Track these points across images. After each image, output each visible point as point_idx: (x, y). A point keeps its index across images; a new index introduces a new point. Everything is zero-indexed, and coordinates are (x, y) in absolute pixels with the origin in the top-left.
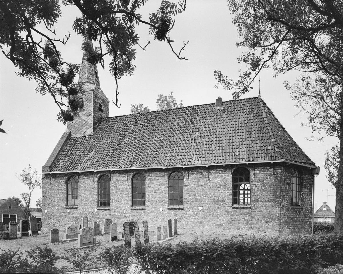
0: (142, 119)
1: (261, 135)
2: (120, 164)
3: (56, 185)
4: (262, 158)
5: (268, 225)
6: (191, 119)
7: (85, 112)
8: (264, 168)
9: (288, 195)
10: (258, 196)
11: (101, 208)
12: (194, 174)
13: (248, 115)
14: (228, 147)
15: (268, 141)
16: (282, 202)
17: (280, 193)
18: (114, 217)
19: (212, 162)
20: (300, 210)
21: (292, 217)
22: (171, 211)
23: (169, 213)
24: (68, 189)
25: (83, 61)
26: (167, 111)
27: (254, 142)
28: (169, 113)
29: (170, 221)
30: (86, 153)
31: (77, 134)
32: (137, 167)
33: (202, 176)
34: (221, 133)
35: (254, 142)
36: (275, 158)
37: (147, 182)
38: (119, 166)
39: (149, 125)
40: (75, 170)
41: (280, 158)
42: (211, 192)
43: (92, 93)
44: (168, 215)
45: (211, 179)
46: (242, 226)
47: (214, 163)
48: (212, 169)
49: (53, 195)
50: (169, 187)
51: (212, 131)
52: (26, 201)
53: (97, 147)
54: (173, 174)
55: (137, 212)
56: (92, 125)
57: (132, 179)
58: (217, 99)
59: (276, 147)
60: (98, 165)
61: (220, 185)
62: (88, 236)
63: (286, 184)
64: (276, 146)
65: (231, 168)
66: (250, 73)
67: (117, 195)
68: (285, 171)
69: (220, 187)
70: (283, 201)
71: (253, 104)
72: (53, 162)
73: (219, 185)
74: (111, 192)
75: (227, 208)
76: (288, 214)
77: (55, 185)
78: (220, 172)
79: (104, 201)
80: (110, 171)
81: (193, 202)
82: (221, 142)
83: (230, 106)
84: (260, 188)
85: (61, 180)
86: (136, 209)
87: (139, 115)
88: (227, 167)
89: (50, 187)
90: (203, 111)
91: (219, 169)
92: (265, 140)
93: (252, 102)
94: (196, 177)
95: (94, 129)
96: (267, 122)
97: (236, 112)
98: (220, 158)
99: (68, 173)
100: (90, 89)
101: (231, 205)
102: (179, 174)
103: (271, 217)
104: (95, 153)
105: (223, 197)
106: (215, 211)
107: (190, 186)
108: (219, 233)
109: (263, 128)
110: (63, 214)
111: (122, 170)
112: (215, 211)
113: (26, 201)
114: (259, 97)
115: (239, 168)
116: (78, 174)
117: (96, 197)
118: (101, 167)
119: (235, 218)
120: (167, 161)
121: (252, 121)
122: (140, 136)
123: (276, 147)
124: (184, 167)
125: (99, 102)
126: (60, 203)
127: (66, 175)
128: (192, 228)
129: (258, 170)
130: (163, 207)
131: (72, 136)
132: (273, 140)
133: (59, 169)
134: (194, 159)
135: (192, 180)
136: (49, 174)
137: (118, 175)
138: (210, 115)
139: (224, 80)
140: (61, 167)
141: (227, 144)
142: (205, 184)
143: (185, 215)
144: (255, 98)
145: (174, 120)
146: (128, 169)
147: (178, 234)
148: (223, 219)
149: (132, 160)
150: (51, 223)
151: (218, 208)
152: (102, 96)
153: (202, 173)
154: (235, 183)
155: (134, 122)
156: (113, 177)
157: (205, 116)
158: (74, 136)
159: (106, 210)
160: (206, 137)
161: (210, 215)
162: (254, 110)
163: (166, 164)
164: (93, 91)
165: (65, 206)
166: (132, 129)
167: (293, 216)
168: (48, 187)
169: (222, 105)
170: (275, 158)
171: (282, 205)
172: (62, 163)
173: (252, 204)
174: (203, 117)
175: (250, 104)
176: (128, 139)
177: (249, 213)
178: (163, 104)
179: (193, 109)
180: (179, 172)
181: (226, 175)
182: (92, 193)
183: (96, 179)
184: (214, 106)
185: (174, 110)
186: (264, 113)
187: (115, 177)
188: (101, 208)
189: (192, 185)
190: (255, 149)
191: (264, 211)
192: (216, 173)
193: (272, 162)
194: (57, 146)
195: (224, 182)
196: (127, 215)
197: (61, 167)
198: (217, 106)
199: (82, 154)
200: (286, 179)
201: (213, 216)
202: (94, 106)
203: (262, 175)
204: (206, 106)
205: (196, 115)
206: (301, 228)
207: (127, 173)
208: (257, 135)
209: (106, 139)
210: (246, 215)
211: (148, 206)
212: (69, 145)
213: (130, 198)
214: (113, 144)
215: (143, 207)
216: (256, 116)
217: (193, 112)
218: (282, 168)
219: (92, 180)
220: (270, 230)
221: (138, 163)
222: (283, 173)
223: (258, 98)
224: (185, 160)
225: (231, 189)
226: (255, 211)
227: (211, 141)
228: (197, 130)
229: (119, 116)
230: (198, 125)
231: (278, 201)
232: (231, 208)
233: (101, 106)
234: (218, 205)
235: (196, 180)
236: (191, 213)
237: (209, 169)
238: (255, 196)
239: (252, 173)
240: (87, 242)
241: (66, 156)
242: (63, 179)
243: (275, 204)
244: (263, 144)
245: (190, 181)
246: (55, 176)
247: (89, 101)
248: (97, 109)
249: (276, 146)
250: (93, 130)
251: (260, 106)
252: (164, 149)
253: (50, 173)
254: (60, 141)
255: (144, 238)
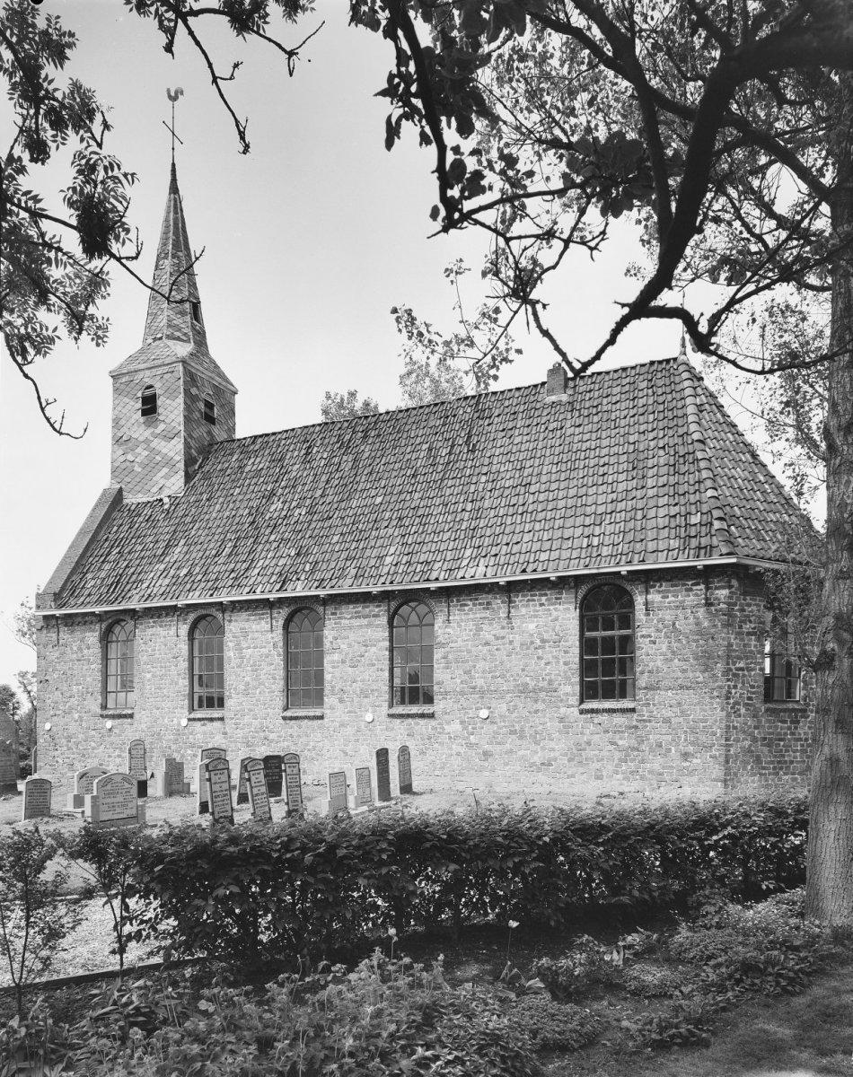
0: (327, 441)
1: (672, 480)
2: (251, 582)
3: (75, 648)
4: (670, 553)
5: (688, 764)
6: (469, 437)
7: (162, 427)
8: (676, 586)
9: (754, 669)
10: (658, 672)
11: (199, 715)
12: (466, 608)
13: (641, 418)
14: (569, 522)
15: (693, 498)
16: (733, 691)
17: (728, 664)
18: (235, 742)
19: (518, 571)
20: (796, 717)
21: (770, 739)
22: (399, 721)
23: (393, 729)
24: (107, 659)
25: (158, 272)
26: (401, 415)
27: (652, 503)
28: (405, 421)
29: (382, 755)
30: (160, 552)
31: (140, 495)
32: (298, 589)
33: (487, 614)
34: (554, 477)
35: (652, 503)
36: (711, 551)
37: (329, 633)
38: (247, 589)
39: (345, 458)
40: (123, 603)
41: (724, 551)
42: (515, 664)
43: (181, 368)
44: (387, 733)
45: (516, 622)
46: (610, 767)
47: (524, 571)
48: (519, 591)
49: (67, 677)
50: (391, 650)
51: (527, 472)
52: (29, 692)
53: (193, 533)
54: (405, 610)
55: (300, 727)
56: (181, 465)
57: (286, 627)
58: (550, 371)
59: (715, 516)
60: (188, 586)
61: (543, 641)
62: (120, 798)
63: (749, 634)
64: (716, 513)
65: (577, 587)
66: (497, 311)
67: (244, 674)
68: (745, 594)
69: (544, 648)
70: (735, 687)
71: (660, 383)
72: (66, 581)
73: (538, 641)
74: (226, 666)
75: (563, 710)
76: (756, 728)
77: (71, 649)
78: (544, 598)
79: (208, 696)
80: (221, 603)
81: (462, 693)
82: (550, 507)
83: (590, 391)
84: (664, 648)
85: (87, 634)
86: (296, 718)
87: (318, 428)
88: (562, 584)
89: (57, 654)
90: (507, 410)
91: (539, 590)
92: (684, 494)
93: (659, 375)
94: (471, 616)
95: (188, 477)
96: (696, 436)
97: (605, 408)
98: (544, 556)
99: (106, 612)
100: (174, 359)
101: (577, 703)
102: (422, 609)
103: (698, 739)
104: (186, 549)
105: (553, 677)
106: (527, 720)
107: (452, 645)
108: (541, 790)
109: (684, 456)
110: (93, 733)
111: (257, 600)
112: (527, 720)
113: (29, 692)
114: (683, 357)
115: (599, 586)
116: (132, 613)
117: (184, 683)
118: (197, 593)
119: (589, 743)
120: (386, 570)
121: (651, 435)
122: (317, 495)
123: (715, 516)
124: (433, 586)
125: (203, 396)
126: (85, 700)
127: (100, 617)
128: (461, 774)
129: (659, 592)
130: (376, 708)
131: (125, 501)
132: (710, 493)
133: (82, 599)
134: (465, 562)
135: (460, 626)
136: (53, 616)
137: (244, 615)
138: (528, 422)
139: (420, 334)
140: (89, 595)
141: (569, 511)
142: (497, 639)
143: (440, 733)
144: (668, 361)
145: (418, 442)
146: (272, 597)
147: (415, 793)
148: (552, 744)
149: (287, 568)
150: (61, 761)
151: (537, 711)
152: (213, 375)
153: (488, 603)
154: (588, 634)
155: (303, 452)
156: (230, 621)
157: (511, 425)
158: (130, 499)
159: (211, 720)
160: (507, 492)
161: (513, 732)
162: (661, 399)
163: (382, 580)
164: (184, 362)
165: (99, 711)
166: (294, 474)
167: (772, 733)
168: (53, 655)
169: (566, 386)
170: (711, 551)
171: (732, 701)
172: (93, 583)
173: (640, 700)
174: (504, 430)
175: (651, 380)
176: (280, 506)
177: (631, 728)
178: (419, 388)
179: (477, 404)
180: (420, 602)
181: (561, 607)
182: (174, 671)
183: (184, 629)
184: (542, 391)
185: (421, 411)
186: (691, 409)
187: (236, 621)
188: (199, 715)
189: (460, 643)
190: (652, 523)
191: (677, 720)
192: (531, 603)
193: (700, 564)
194: (82, 532)
195: (554, 630)
196: (272, 736)
197: (89, 595)
198: (551, 392)
199: (148, 553)
200: (745, 616)
201: (521, 737)
202: (188, 408)
203: (670, 608)
204: (517, 394)
205: (486, 423)
206: (800, 774)
207: (271, 608)
208: (662, 480)
209: (218, 507)
210: (622, 732)
211: (332, 708)
212: (115, 528)
213: (281, 684)
214: (237, 520)
215: (318, 713)
216: (666, 420)
217: (476, 415)
218: (735, 583)
219: (173, 631)
220: (695, 779)
221: (303, 578)
222: (738, 599)
223: (679, 361)
224: (437, 565)
225: (577, 651)
226: (650, 721)
227: (521, 502)
228: (485, 470)
229: (261, 436)
230: (488, 455)
231: (720, 687)
232: (576, 711)
233: (209, 406)
234: (536, 701)
235: (471, 625)
236: (455, 727)
237: (511, 589)
238: (649, 672)
239: (639, 600)
240: (116, 817)
241: (103, 562)
242: (93, 631)
243: (711, 698)
244: (677, 508)
245: (455, 631)
246: (69, 621)
247: (171, 395)
248: (196, 415)
249: (716, 513)
250: (183, 480)
251: (681, 386)
252: (382, 532)
253: (57, 613)
254: (91, 516)
255: (287, 804)
